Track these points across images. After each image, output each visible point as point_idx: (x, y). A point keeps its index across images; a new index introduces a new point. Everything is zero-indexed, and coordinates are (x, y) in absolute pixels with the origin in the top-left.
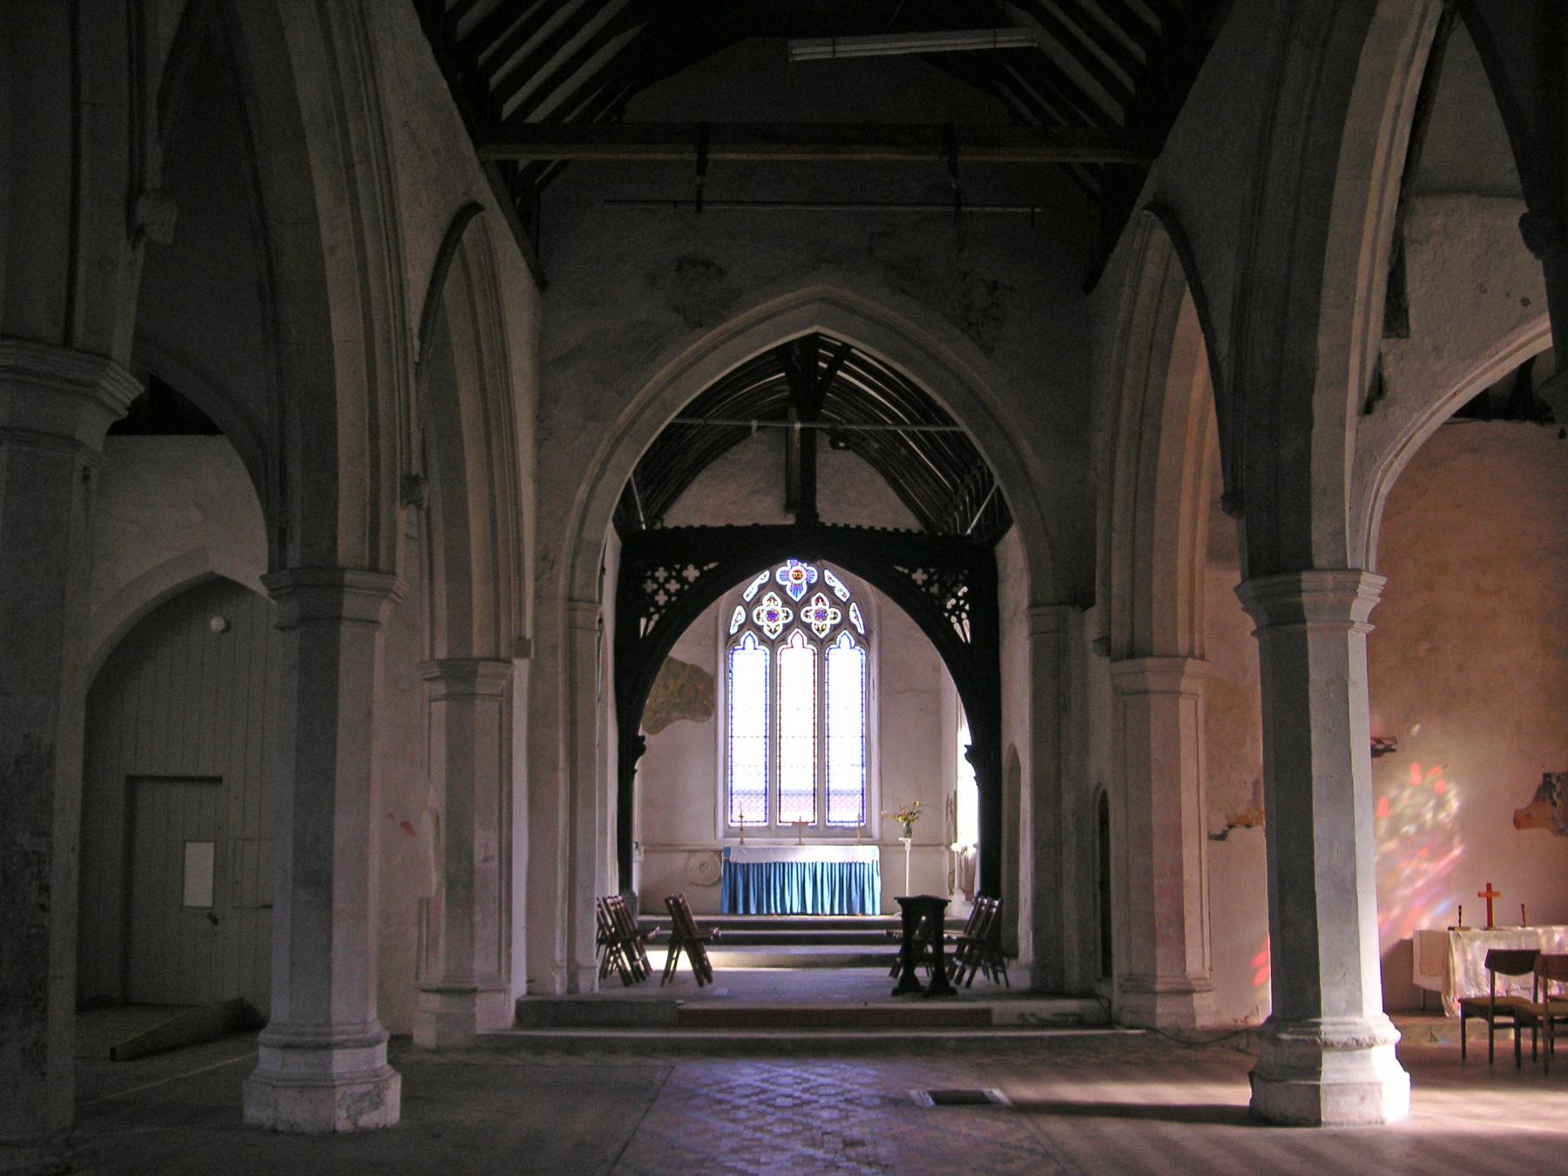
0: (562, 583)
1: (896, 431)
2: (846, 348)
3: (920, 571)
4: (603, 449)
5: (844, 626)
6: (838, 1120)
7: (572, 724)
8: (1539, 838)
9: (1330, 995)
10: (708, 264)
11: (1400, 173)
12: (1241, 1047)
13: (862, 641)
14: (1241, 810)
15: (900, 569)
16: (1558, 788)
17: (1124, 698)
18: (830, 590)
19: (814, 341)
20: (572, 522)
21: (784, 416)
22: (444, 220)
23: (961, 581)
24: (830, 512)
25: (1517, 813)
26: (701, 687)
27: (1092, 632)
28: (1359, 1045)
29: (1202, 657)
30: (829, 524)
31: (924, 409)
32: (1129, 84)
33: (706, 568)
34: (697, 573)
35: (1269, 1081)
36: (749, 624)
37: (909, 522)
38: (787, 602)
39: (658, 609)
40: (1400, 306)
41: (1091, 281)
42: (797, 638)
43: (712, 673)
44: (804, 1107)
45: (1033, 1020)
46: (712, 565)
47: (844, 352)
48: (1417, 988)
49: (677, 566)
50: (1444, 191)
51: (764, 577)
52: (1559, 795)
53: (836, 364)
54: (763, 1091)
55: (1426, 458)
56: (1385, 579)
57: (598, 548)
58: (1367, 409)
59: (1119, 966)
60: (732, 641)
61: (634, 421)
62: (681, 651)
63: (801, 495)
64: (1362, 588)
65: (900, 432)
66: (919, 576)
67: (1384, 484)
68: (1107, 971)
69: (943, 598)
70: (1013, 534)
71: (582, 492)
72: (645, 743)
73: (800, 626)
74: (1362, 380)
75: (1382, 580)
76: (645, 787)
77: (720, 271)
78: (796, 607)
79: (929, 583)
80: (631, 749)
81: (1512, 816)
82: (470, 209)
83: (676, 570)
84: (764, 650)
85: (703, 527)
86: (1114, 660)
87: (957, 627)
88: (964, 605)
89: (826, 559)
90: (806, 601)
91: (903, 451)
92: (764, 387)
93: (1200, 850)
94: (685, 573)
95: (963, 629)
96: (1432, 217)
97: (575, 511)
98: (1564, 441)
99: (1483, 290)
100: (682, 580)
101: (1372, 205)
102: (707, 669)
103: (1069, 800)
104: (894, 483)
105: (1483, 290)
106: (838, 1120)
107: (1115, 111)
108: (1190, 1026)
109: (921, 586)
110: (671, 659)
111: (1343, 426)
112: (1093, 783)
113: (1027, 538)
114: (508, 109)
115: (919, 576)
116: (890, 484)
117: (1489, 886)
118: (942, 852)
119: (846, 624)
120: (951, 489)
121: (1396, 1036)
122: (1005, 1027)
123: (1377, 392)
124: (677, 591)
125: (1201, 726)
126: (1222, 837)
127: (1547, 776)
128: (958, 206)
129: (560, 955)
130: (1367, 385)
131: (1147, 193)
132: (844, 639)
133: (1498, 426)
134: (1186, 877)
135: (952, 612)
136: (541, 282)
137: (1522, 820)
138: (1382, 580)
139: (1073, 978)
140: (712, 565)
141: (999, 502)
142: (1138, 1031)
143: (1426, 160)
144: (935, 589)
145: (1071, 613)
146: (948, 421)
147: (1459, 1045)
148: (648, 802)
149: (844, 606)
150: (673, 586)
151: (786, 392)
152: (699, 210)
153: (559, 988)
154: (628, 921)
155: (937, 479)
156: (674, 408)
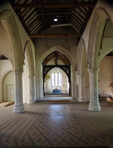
10: (48, 45)
14: (88, 86)
19: (56, 51)
20: (12, 46)
22: (26, 42)
24: (58, 64)
27: (77, 73)
31: (65, 56)
32: (80, 30)
37: (64, 64)
41: (77, 46)
42: (56, 73)
47: (59, 52)
50: (105, 37)
51: (54, 68)
53: (58, 53)
55: (103, 59)
57: (40, 67)
58: (98, 55)
61: (43, 57)
62: (48, 74)
63: (56, 63)
64: (98, 70)
66: (65, 68)
67: (100, 61)
69: (66, 70)
71: (39, 63)
75: (99, 69)
76: (45, 83)
79: (65, 69)
80: (44, 81)
82: (28, 41)
84: (54, 74)
95: (68, 72)
100: (47, 69)
101: (99, 38)
103: (75, 85)
104: (63, 61)
107: (79, 32)
113: (73, 67)
114: (32, 33)
115: (65, 68)
121: (100, 104)
126: (87, 88)
128: (46, 36)
129: (38, 97)
131: (81, 39)
133: (108, 56)
136: (35, 47)
138: (99, 69)
141: (70, 63)
143: (104, 34)
144: (66, 69)
150: (47, 70)
153: (38, 99)
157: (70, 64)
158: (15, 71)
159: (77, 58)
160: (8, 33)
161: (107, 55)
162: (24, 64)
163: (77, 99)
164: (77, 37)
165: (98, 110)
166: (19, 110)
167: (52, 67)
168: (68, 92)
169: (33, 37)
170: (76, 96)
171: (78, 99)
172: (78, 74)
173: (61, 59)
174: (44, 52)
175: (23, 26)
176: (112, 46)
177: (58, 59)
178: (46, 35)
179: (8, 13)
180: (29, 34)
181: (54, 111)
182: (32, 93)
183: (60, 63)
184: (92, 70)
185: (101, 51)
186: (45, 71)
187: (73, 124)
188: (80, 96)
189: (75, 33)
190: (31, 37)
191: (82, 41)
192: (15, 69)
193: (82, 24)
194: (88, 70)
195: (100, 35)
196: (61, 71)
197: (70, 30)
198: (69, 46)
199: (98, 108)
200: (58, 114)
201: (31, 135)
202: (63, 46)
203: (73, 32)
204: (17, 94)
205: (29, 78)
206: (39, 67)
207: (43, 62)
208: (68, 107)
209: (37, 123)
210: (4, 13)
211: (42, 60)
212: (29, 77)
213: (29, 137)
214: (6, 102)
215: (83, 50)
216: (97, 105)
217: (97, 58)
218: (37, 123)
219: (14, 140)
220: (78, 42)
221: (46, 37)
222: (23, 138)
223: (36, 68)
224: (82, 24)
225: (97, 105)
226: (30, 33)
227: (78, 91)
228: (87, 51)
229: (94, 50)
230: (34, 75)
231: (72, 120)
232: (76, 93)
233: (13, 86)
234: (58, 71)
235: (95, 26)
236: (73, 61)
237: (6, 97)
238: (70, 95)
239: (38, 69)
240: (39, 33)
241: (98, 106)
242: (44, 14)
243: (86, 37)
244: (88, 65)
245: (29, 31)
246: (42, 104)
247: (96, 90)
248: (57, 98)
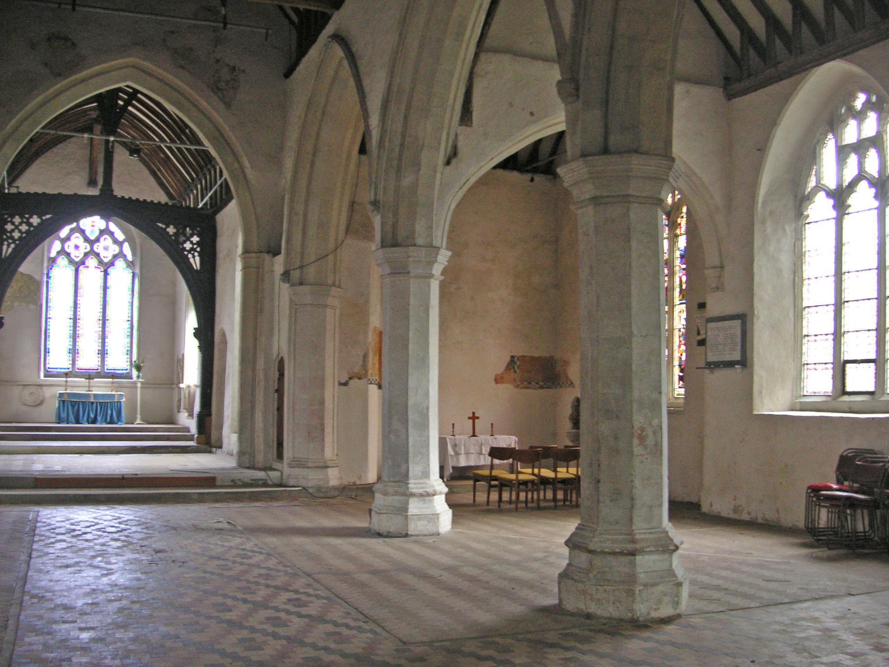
1: (161, 146)
2: (136, 91)
3: (172, 227)
5: (120, 255)
6: (146, 538)
9: (414, 469)
10: (66, 39)
11: (477, 40)
12: (353, 497)
13: (130, 265)
14: (356, 370)
15: (160, 225)
16: (518, 363)
17: (296, 307)
18: (112, 234)
21: (89, 129)
23: (183, 231)
24: (119, 191)
25: (497, 375)
26: (32, 288)
28: (428, 495)
29: (340, 287)
30: (119, 196)
31: (180, 130)
33: (44, 218)
34: (39, 220)
35: (381, 514)
36: (63, 252)
37: (161, 197)
38: (87, 239)
39: (14, 241)
40: (468, 109)
41: (288, 74)
43: (39, 280)
44: (40, 542)
45: (239, 483)
46: (48, 216)
47: (133, 95)
49: (27, 216)
50: (497, 51)
51: (74, 225)
52: (518, 367)
53: (128, 103)
54: (97, 524)
56: (451, 253)
58: (448, 163)
59: (287, 453)
60: (53, 261)
62: (26, 267)
65: (174, 148)
66: (171, 230)
68: (280, 456)
72: (3, 321)
73: (93, 254)
74: (446, 147)
75: (449, 253)
77: (73, 44)
78: (92, 243)
81: (493, 377)
83: (25, 218)
85: (44, 193)
86: (292, 285)
87: (192, 260)
88: (197, 248)
90: (97, 240)
91: (162, 155)
92: (77, 112)
93: (158, 384)
94: (31, 220)
96: (490, 64)
98: (532, 184)
99: (511, 105)
100: (30, 224)
102: (37, 277)
105: (511, 105)
106: (146, 538)
108: (327, 486)
109: (172, 236)
110: (22, 274)
111: (435, 172)
112: (275, 351)
116: (152, 174)
117: (474, 413)
118: (173, 388)
119: (121, 255)
120: (190, 180)
122: (222, 487)
123: (453, 155)
124: (27, 230)
125: (337, 324)
126: (345, 384)
127: (513, 357)
130: (448, 152)
131: (329, 29)
132: (120, 264)
134: (326, 405)
135: (189, 252)
137: (498, 380)
138: (449, 253)
139: (260, 459)
140: (48, 216)
142: (298, 488)
145: (267, 257)
147: (477, 494)
149: (120, 244)
150: (24, 228)
151: (94, 114)
152: (74, 9)
155: (181, 173)
156: (40, 124)
159: (289, 163)
161: (510, 164)
171: (276, 465)
176: (532, 114)
191: (338, 52)
198: (233, 69)
199: (435, 517)
216: (430, 490)
217: (438, 175)
234: (106, 249)
244: (828, 505)
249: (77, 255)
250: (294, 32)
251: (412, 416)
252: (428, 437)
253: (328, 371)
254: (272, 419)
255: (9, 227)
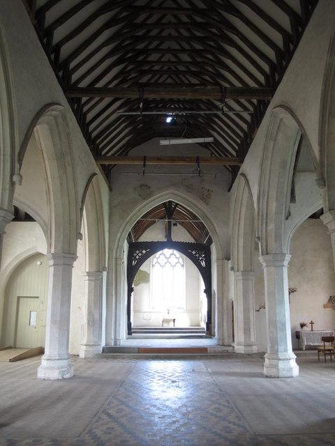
0: (114, 255)
4: (124, 225)
7: (116, 285)
8: (329, 310)
9: (281, 348)
19: (170, 202)
20: (117, 241)
24: (174, 238)
27: (230, 266)
31: (195, 217)
32: (237, 148)
36: (157, 262)
37: (192, 240)
41: (229, 191)
42: (168, 264)
47: (177, 204)
48: (300, 370)
50: (304, 171)
62: (143, 268)
66: (194, 253)
70: (213, 244)
78: (168, 258)
79: (195, 254)
80: (130, 290)
82: (95, 174)
89: (176, 250)
97: (118, 239)
107: (234, 154)
115: (194, 253)
128: (145, 162)
129: (113, 337)
131: (240, 172)
132: (178, 265)
136: (111, 189)
143: (300, 164)
145: (225, 261)
146: (198, 219)
148: (135, 301)
149: (178, 259)
150: (140, 255)
153: (112, 344)
154: (264, 225)
157: (210, 241)
158: (54, 256)
160: (45, 155)
161: (310, 217)
162: (79, 236)
163: (229, 346)
164: (230, 166)
165: (289, 374)
166: (57, 371)
167: (153, 248)
168: (204, 325)
169: (107, 163)
170: (226, 335)
172: (232, 269)
173: (182, 224)
174: (134, 203)
175: (84, 136)
177: (175, 225)
178: (145, 159)
179: (53, 110)
180: (97, 153)
181: (160, 376)
182: (94, 322)
183: (181, 235)
184: (269, 257)
185: (292, 205)
186: (135, 259)
187: (215, 408)
188: (240, 336)
189: (225, 154)
190: (102, 165)
191: (242, 178)
192: (53, 251)
193: (242, 134)
194: (261, 259)
195: (288, 167)
196: (183, 260)
197: (215, 130)
199: (291, 369)
200: (174, 384)
201: (98, 432)
202: (189, 188)
203: (221, 156)
204: (53, 322)
205: (87, 277)
206: (120, 247)
207: (130, 234)
208: (204, 366)
209: (103, 424)
210: (51, 108)
211: (129, 228)
212: (89, 274)
213: (95, 437)
214: (10, 348)
215: (245, 202)
218: (103, 424)
219: (51, 443)
220: (233, 182)
221: (144, 165)
222: (78, 438)
223: (109, 249)
224: (242, 134)
225: (287, 359)
226: (101, 154)
227: (233, 321)
228: (255, 205)
229: (273, 206)
230: (104, 269)
231: (214, 399)
232: (228, 326)
233: (37, 299)
235: (274, 143)
236: (219, 232)
237: (12, 333)
238: (209, 332)
239: (116, 254)
240: (124, 152)
241: (291, 361)
242: (143, 113)
243: (250, 167)
245: (98, 147)
246: (123, 358)
247: (284, 316)
248: (168, 341)
249: (162, 264)
250: (231, 174)
251: (279, 325)
252: (286, 334)
253: (251, 306)
254: (230, 325)
255: (135, 255)
